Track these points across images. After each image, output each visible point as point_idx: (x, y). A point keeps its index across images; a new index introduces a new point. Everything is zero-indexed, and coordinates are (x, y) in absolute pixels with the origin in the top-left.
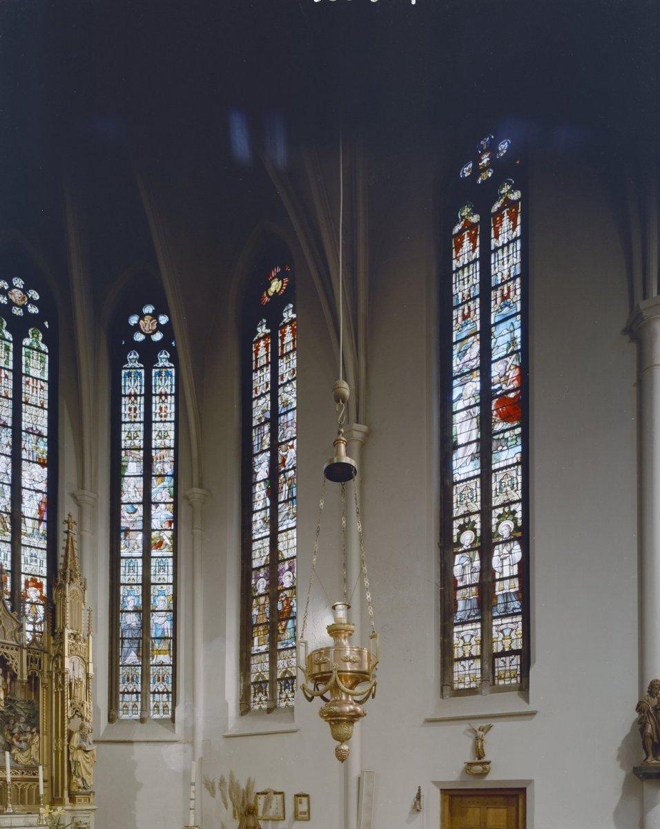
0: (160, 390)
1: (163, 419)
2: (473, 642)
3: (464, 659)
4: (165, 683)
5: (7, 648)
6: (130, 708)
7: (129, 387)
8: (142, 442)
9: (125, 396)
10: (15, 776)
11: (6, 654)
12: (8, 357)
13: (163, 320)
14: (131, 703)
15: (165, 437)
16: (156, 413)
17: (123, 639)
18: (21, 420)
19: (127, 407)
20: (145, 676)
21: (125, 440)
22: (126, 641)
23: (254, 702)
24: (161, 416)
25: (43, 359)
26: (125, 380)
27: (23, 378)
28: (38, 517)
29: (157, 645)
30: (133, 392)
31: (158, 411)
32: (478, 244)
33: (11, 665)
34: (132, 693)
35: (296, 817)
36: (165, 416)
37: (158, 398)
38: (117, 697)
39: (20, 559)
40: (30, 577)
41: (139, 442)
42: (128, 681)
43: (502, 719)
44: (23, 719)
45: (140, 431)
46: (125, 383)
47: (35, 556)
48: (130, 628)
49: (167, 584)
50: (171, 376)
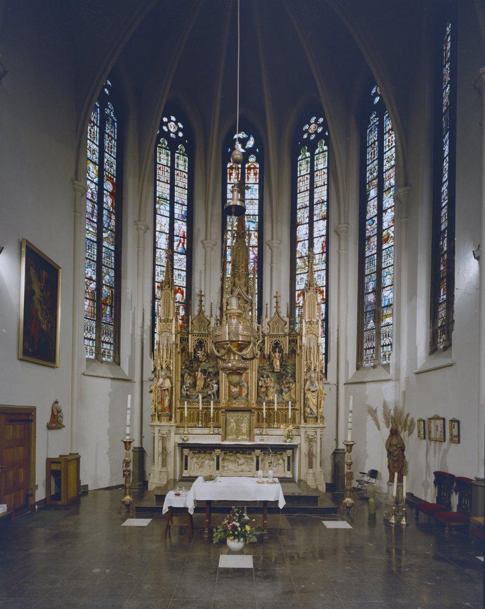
4: (390, 338)
5: (203, 336)
6: (370, 359)
11: (278, 340)
12: (168, 159)
14: (88, 347)
17: (366, 312)
18: (174, 196)
20: (378, 334)
22: (368, 313)
23: (440, 342)
27: (176, 171)
28: (321, 251)
29: (385, 311)
33: (281, 346)
34: (371, 348)
35: (451, 440)
38: (362, 352)
39: (295, 282)
44: (290, 375)
47: (320, 276)
48: (370, 304)
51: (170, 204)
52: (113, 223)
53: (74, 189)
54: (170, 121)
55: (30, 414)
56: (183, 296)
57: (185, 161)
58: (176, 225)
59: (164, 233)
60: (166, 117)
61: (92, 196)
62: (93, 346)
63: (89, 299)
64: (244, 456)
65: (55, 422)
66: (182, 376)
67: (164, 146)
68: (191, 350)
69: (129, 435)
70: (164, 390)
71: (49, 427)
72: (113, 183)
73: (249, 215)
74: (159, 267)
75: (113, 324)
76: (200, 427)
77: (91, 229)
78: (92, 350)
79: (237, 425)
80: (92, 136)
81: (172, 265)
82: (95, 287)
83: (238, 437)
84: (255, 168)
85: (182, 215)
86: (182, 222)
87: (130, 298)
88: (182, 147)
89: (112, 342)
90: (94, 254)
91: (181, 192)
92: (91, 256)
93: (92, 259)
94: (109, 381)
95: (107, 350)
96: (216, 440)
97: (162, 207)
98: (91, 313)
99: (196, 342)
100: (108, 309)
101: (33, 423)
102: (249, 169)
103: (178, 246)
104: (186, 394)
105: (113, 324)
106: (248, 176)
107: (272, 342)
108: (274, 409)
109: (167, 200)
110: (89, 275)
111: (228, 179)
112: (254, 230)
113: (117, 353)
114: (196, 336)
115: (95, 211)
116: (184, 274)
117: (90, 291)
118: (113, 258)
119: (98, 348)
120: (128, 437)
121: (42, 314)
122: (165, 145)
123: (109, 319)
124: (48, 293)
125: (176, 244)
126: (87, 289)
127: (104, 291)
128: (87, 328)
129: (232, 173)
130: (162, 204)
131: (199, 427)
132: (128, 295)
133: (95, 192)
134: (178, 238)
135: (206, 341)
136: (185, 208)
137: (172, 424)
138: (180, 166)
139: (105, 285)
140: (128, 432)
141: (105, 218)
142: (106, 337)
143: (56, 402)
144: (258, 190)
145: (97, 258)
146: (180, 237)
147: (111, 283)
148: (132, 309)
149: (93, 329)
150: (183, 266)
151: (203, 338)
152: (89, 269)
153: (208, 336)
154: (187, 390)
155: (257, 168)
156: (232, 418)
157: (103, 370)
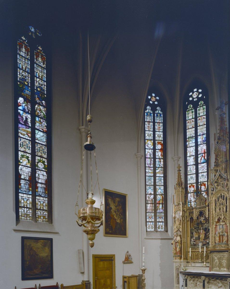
0: (148, 120)
1: (159, 131)
2: (44, 204)
3: (40, 209)
5: (202, 208)
7: (148, 119)
8: (162, 138)
9: (156, 122)
10: (192, 251)
11: (202, 210)
14: (150, 226)
16: (147, 128)
19: (157, 126)
21: (147, 137)
24: (158, 130)
26: (156, 117)
30: (149, 121)
31: (157, 128)
34: (151, 222)
36: (160, 130)
37: (147, 123)
41: (152, 138)
42: (160, 218)
43: (27, 232)
45: (151, 134)
46: (146, 117)
47: (192, 177)
49: (152, 185)
50: (161, 117)
52: (162, 163)
55: (112, 257)
61: (150, 156)
62: (153, 225)
63: (150, 203)
64: (223, 281)
65: (128, 260)
66: (192, 233)
68: (195, 217)
69: (144, 266)
70: (176, 243)
71: (124, 263)
72: (161, 145)
74: (201, 173)
75: (164, 212)
76: (200, 263)
77: (150, 171)
78: (153, 227)
79: (220, 261)
83: (220, 269)
85: (203, 140)
87: (171, 197)
89: (163, 221)
90: (162, 183)
93: (151, 185)
94: (160, 240)
95: (150, 226)
96: (206, 271)
97: (190, 142)
99: (199, 212)
101: (113, 261)
103: (201, 159)
104: (193, 243)
105: (164, 212)
108: (199, 251)
110: (150, 192)
113: (166, 227)
117: (150, 200)
119: (155, 226)
120: (143, 268)
121: (117, 216)
123: (161, 211)
124: (120, 207)
127: (158, 198)
128: (150, 217)
131: (199, 263)
132: (170, 196)
135: (204, 211)
137: (181, 261)
139: (159, 195)
140: (143, 265)
141: (157, 163)
142: (160, 219)
143: (128, 252)
145: (154, 184)
147: (162, 192)
149: (152, 217)
150: (205, 169)
151: (202, 209)
152: (150, 190)
154: (194, 241)
156: (216, 257)
157: (158, 236)
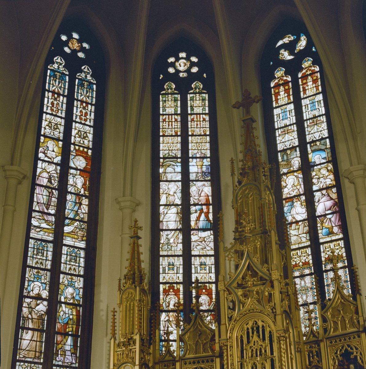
1: (83, 122)
5: (203, 362)
13: (64, 38)
15: (84, 138)
19: (79, 110)
25: (176, 99)
31: (78, 113)
32: (291, 93)
33: (356, 357)
40: (167, 285)
46: (78, 90)
47: (173, 265)
51: (181, 162)
52: (85, 209)
53: (6, 178)
54: (178, 59)
56: (211, 298)
57: (203, 100)
58: (193, 190)
59: (173, 205)
60: (64, 34)
67: (170, 91)
73: (313, 141)
74: (166, 258)
77: (44, 225)
80: (55, 109)
81: (190, 250)
82: (44, 309)
84: (314, 72)
85: (203, 172)
86: (203, 183)
88: (197, 85)
91: (199, 141)
92: (41, 263)
97: (169, 169)
98: (36, 351)
100: (70, 341)
102: (305, 77)
106: (304, 88)
107: (336, 353)
109: (177, 158)
110: (36, 291)
111: (274, 103)
112: (324, 161)
114: (190, 363)
115: (53, 199)
116: (210, 261)
117: (35, 316)
118: (82, 260)
122: (171, 89)
125: (193, 217)
126: (30, 313)
129: (279, 92)
130: (168, 166)
132: (102, 313)
133: (55, 175)
134: (198, 207)
136: (207, 162)
138: (195, 109)
141: (69, 205)
144: (322, 102)
145: (52, 265)
146: (202, 205)
147: (77, 298)
148: (107, 334)
150: (208, 248)
152: (36, 283)
153: (212, 361)
155: (317, 72)
